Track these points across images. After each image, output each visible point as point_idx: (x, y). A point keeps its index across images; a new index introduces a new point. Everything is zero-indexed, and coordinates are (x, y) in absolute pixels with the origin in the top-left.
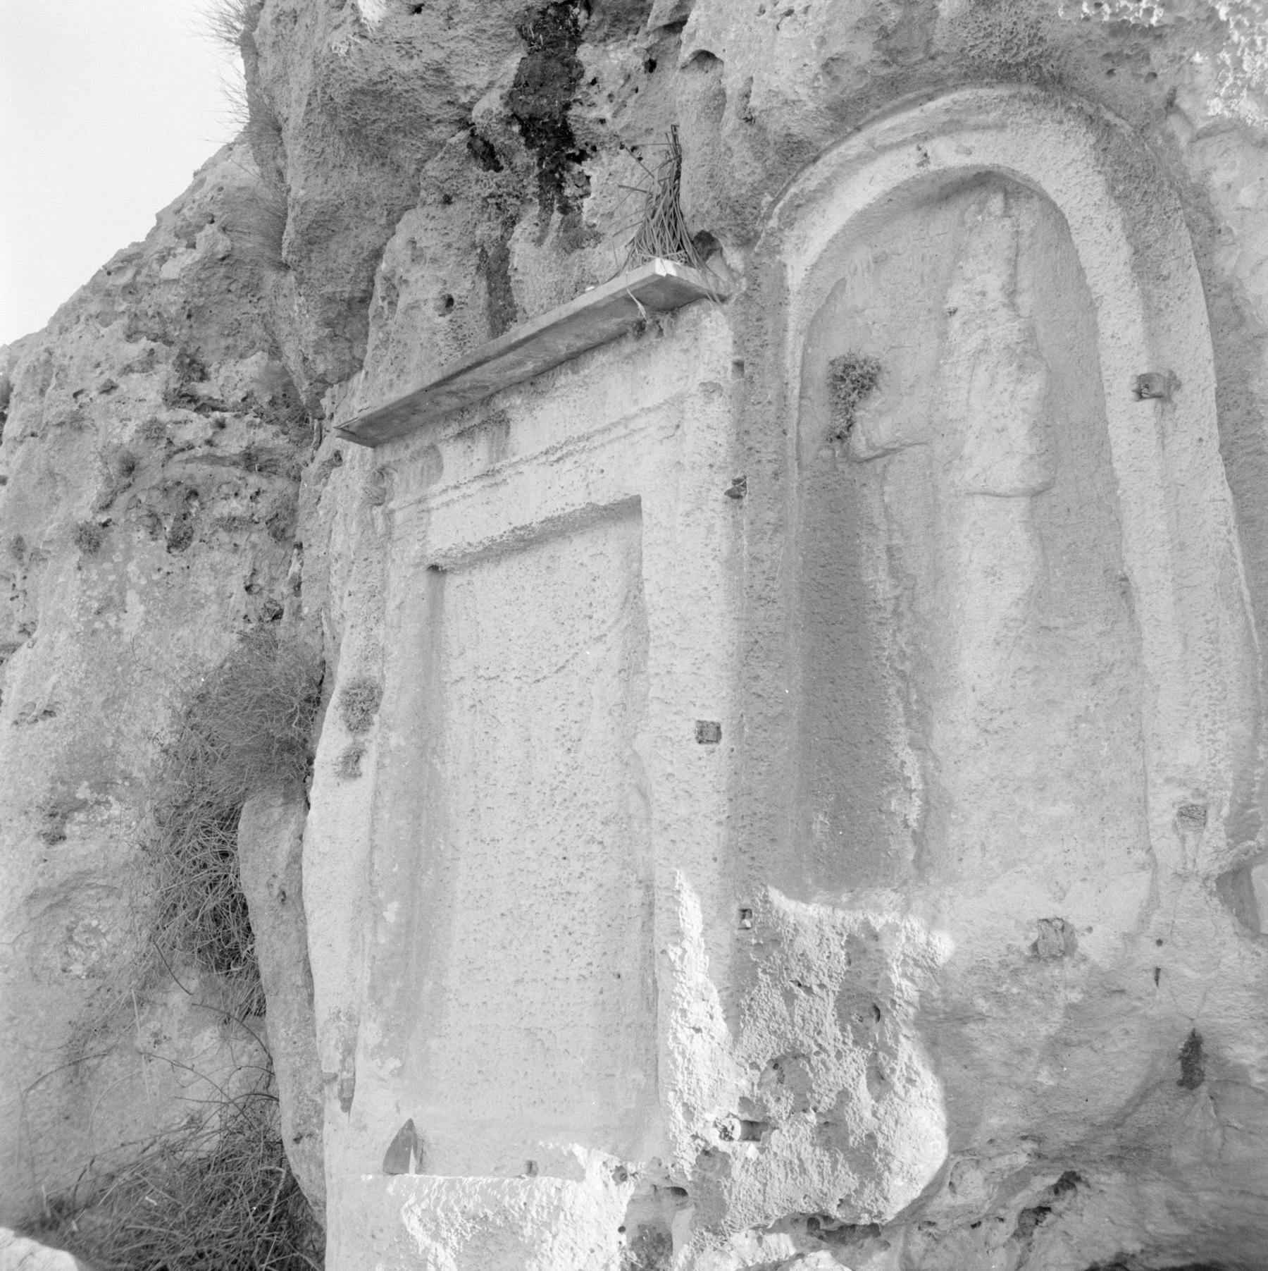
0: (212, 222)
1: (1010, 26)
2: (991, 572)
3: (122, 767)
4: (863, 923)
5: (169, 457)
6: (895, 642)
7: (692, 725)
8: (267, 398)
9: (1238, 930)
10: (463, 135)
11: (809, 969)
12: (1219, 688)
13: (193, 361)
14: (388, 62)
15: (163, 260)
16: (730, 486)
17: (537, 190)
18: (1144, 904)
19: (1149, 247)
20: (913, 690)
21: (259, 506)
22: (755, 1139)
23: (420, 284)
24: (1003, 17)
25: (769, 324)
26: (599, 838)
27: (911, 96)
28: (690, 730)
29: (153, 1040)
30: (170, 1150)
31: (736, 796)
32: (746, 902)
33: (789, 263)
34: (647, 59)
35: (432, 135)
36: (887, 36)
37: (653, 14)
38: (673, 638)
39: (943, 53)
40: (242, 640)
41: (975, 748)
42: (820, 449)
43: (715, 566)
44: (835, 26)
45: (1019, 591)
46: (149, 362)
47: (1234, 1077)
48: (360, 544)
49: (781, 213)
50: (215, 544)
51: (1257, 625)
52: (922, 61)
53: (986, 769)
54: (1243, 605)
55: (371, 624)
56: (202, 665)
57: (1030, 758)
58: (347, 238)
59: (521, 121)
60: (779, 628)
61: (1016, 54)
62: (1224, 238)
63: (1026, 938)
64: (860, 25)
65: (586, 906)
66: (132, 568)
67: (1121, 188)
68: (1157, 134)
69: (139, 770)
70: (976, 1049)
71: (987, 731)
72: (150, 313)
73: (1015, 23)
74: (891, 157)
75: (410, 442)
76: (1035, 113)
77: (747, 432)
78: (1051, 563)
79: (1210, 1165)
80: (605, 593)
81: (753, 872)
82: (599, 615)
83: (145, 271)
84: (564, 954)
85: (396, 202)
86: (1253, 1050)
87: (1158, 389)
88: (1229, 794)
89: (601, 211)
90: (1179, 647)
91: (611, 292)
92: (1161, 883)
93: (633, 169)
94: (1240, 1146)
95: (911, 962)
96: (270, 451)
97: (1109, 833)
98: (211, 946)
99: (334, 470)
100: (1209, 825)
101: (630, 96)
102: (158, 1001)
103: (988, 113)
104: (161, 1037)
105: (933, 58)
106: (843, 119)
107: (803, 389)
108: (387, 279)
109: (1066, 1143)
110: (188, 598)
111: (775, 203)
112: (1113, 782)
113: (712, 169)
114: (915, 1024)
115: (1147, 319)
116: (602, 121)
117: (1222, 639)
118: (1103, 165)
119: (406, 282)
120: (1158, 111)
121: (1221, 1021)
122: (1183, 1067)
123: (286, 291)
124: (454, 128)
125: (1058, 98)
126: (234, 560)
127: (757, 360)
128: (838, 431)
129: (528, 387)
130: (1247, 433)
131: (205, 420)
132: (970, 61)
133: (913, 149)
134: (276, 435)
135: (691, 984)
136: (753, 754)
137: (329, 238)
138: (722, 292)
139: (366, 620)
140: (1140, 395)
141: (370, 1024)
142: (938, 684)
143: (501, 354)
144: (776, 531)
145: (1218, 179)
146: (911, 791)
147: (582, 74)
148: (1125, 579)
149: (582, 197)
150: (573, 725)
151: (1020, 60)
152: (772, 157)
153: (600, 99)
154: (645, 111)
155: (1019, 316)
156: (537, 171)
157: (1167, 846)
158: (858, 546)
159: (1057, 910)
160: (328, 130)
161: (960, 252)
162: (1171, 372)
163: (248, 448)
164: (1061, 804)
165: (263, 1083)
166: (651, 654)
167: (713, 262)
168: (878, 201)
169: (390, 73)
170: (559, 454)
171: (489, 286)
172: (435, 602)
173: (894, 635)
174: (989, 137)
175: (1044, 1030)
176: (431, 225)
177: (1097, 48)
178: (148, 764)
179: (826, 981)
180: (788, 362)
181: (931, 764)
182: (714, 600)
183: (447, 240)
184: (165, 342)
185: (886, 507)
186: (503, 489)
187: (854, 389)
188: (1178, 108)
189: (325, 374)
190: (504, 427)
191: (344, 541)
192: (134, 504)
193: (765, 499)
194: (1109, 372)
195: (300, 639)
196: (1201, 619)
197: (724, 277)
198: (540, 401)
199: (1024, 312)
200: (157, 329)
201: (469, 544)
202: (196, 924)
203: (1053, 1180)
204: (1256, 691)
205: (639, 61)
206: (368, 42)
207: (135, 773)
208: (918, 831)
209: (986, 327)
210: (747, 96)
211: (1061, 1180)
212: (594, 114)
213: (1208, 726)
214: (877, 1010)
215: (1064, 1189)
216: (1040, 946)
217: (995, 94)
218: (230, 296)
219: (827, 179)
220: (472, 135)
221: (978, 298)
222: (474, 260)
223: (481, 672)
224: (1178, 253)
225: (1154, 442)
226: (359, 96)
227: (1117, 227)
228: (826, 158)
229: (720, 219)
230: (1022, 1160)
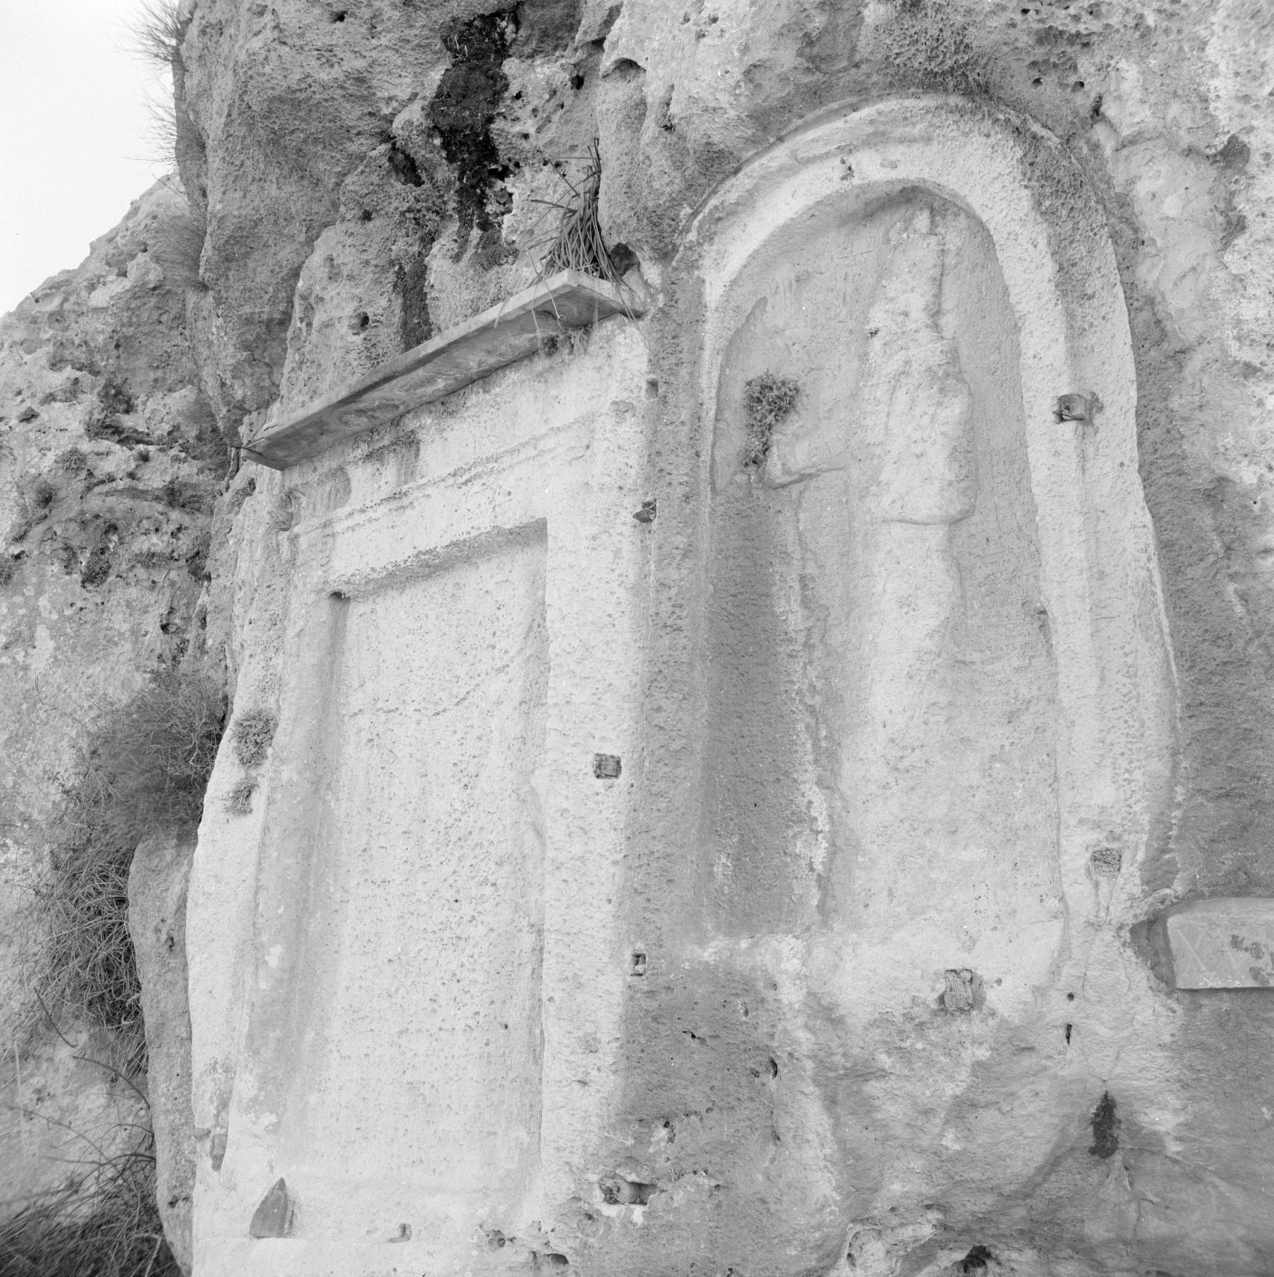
0: (145, 251)
1: (936, 33)
2: (906, 603)
3: (22, 808)
5: (89, 489)
6: (805, 674)
7: (590, 758)
8: (194, 433)
9: (1153, 984)
10: (383, 148)
12: (1137, 725)
13: (119, 393)
14: (308, 70)
15: (92, 287)
16: (639, 509)
17: (455, 205)
18: (1056, 954)
19: (1074, 265)
20: (822, 727)
21: (180, 542)
22: (643, 1203)
23: (336, 302)
24: (928, 24)
25: (685, 341)
27: (835, 105)
28: (588, 763)
29: (35, 1097)
30: (45, 1213)
31: (634, 834)
32: (640, 947)
33: (707, 278)
35: (353, 147)
37: (581, 29)
38: (573, 667)
39: (868, 60)
40: (155, 680)
41: (884, 787)
42: (735, 474)
43: (621, 593)
44: (759, 33)
45: (933, 623)
46: (73, 392)
47: (1150, 1145)
48: (264, 570)
49: (700, 227)
50: (132, 580)
51: (1176, 657)
52: (845, 69)
54: (1162, 637)
55: (270, 653)
56: (112, 704)
57: (942, 798)
58: (265, 255)
59: (442, 134)
60: (685, 658)
61: (943, 62)
62: (1148, 249)
63: (933, 989)
64: (784, 31)
65: (476, 951)
66: (43, 602)
67: (1048, 203)
68: (1082, 143)
69: (40, 812)
70: (877, 1109)
71: (897, 769)
72: (77, 342)
73: (941, 30)
75: (318, 464)
76: (962, 125)
77: (658, 453)
78: (969, 594)
79: (1125, 1243)
80: (509, 622)
81: (648, 915)
82: (502, 645)
83: (73, 299)
84: (451, 1002)
85: (315, 217)
86: (1168, 1116)
87: (1079, 410)
88: (1145, 837)
89: (521, 228)
91: (521, 304)
92: (1073, 932)
93: (555, 186)
94: (1156, 1222)
96: (194, 486)
97: (1021, 881)
98: (102, 998)
99: (247, 499)
100: (1123, 870)
101: (555, 111)
102: (45, 1056)
103: (914, 124)
104: (45, 1094)
105: (857, 66)
107: (719, 411)
108: (304, 298)
109: (973, 1213)
110: (101, 636)
111: (695, 214)
113: (630, 180)
114: (814, 1081)
115: (1070, 338)
116: (526, 136)
117: (1140, 673)
118: (1030, 179)
119: (322, 299)
120: (1083, 121)
121: (1135, 1083)
122: (1095, 1133)
123: (205, 313)
124: (374, 140)
125: (985, 109)
126: (151, 597)
127: (672, 379)
128: (753, 455)
130: (1167, 452)
131: (129, 453)
133: (837, 162)
134: (201, 471)
137: (246, 256)
138: (640, 308)
139: (265, 649)
140: (1061, 418)
141: (246, 1076)
142: (848, 720)
143: (409, 369)
144: (685, 556)
145: (1142, 189)
146: (818, 832)
147: (506, 87)
148: (1044, 612)
149: (503, 214)
150: (471, 759)
151: (946, 68)
152: (691, 167)
153: (524, 113)
154: (570, 127)
155: (942, 338)
157: (1079, 892)
158: (772, 575)
159: (958, 959)
160: (248, 141)
161: (884, 271)
162: (1093, 394)
163: (172, 482)
164: (972, 847)
165: (146, 1145)
166: (550, 684)
167: (631, 277)
168: (800, 216)
169: (310, 80)
170: (466, 477)
171: (404, 304)
172: (337, 632)
173: (804, 668)
174: (916, 149)
175: (950, 1090)
176: (349, 242)
177: (1023, 56)
178: (50, 806)
180: (704, 381)
181: (838, 804)
183: (365, 257)
184: (90, 372)
185: (800, 535)
186: (409, 512)
187: (771, 411)
188: (1104, 117)
189: (243, 400)
190: (414, 448)
191: (249, 568)
192: (49, 536)
193: (674, 522)
194: (1030, 394)
195: (202, 674)
196: (1120, 652)
197: (641, 293)
198: (451, 421)
199: (948, 334)
200: (83, 357)
201: (373, 570)
202: (86, 974)
203: (961, 1256)
204: (1174, 728)
205: (565, 77)
206: (287, 49)
207: (35, 816)
209: (907, 349)
210: (668, 105)
211: (969, 1256)
212: (518, 128)
213: (1125, 764)
214: (774, 1065)
215: (974, 1266)
216: (947, 998)
217: (921, 105)
218: (160, 327)
219: (748, 191)
220: (394, 148)
221: (900, 319)
222: (391, 277)
223: (380, 704)
225: (1074, 466)
226: (276, 104)
227: (1042, 242)
228: (747, 170)
229: (637, 230)
230: (927, 1231)
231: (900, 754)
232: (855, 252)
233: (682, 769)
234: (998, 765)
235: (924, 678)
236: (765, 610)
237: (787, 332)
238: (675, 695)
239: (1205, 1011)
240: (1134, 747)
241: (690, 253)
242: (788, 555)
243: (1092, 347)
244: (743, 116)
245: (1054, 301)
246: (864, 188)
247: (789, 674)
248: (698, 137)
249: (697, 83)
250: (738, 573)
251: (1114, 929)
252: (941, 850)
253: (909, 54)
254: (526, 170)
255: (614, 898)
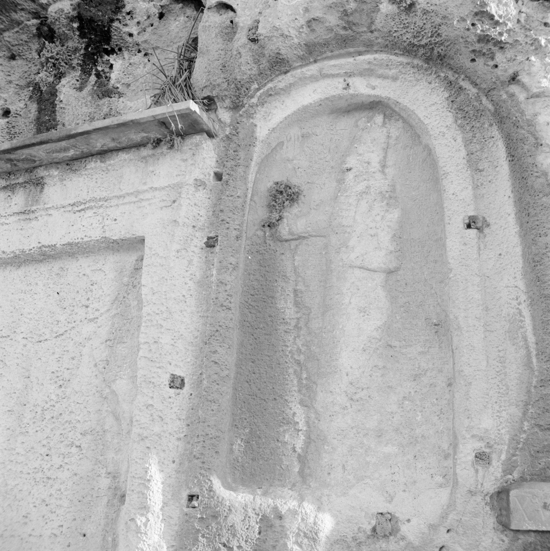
2: (363, 311)
4: (273, 508)
6: (294, 343)
10: (35, 21)
11: (234, 535)
12: (504, 388)
18: (445, 507)
20: (304, 372)
25: (242, 154)
26: (78, 444)
27: (351, 50)
28: (166, 379)
31: (192, 423)
33: (259, 124)
34: (160, 11)
35: (15, 16)
36: (347, 15)
41: (344, 409)
42: (257, 230)
43: (191, 283)
45: (379, 323)
49: (260, 96)
51: (537, 355)
53: (349, 421)
57: (375, 417)
61: (421, 40)
62: (544, 149)
64: (332, 5)
71: (352, 399)
73: (424, 24)
74: (328, 81)
76: (417, 75)
77: (222, 211)
81: (203, 472)
88: (506, 447)
89: (123, 81)
90: (484, 363)
93: (145, 64)
95: (302, 534)
101: (149, 26)
103: (390, 69)
105: (372, 32)
106: (310, 53)
107: (252, 195)
111: (258, 89)
112: (423, 436)
116: (131, 35)
117: (508, 361)
124: (30, 16)
129: (65, 166)
132: (393, 38)
133: (341, 80)
135: (150, 542)
136: (209, 398)
140: (469, 226)
144: (234, 269)
146: (299, 431)
152: (265, 63)
156: (82, 52)
161: (354, 140)
168: (315, 103)
170: (82, 207)
173: (295, 338)
174: (386, 83)
179: (243, 544)
181: (313, 416)
182: (188, 303)
183: (9, 78)
185: (295, 269)
186: (34, 222)
190: (39, 188)
193: (230, 250)
194: (450, 212)
198: (71, 175)
205: (155, 11)
208: (302, 454)
212: (126, 29)
213: (497, 408)
219: (290, 84)
224: (489, 159)
225: (476, 252)
227: (460, 139)
231: (355, 391)
232: (338, 128)
233: (225, 387)
234: (407, 402)
235: (372, 352)
236: (271, 305)
237: (295, 161)
238: (225, 345)
239: (520, 541)
240: (502, 399)
241: (251, 109)
242: (287, 277)
243: (483, 195)
244: (302, 43)
245: (466, 169)
246: (352, 96)
247: (285, 342)
248: (274, 48)
249: (279, 21)
250: (255, 283)
251: (483, 495)
252: (372, 446)
253: (402, 33)
254: (126, 54)
255: (177, 461)
